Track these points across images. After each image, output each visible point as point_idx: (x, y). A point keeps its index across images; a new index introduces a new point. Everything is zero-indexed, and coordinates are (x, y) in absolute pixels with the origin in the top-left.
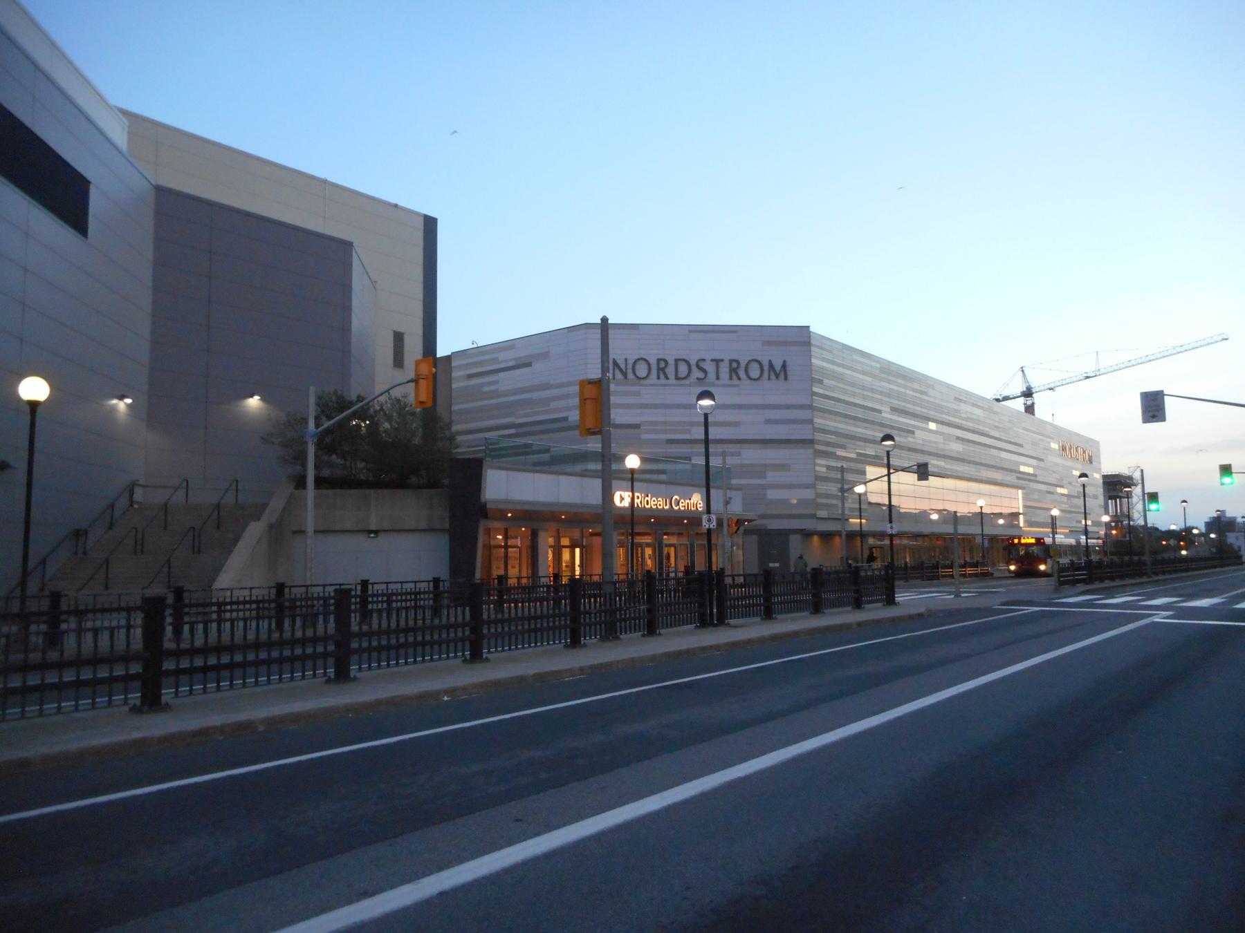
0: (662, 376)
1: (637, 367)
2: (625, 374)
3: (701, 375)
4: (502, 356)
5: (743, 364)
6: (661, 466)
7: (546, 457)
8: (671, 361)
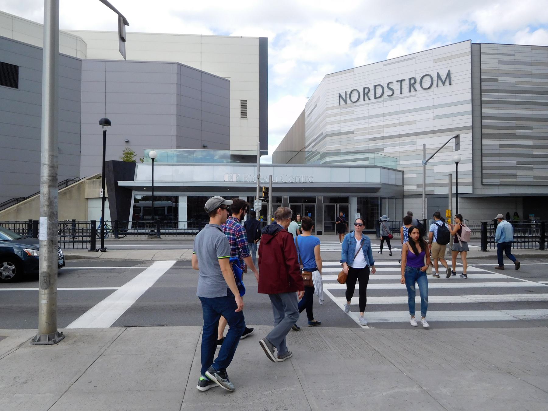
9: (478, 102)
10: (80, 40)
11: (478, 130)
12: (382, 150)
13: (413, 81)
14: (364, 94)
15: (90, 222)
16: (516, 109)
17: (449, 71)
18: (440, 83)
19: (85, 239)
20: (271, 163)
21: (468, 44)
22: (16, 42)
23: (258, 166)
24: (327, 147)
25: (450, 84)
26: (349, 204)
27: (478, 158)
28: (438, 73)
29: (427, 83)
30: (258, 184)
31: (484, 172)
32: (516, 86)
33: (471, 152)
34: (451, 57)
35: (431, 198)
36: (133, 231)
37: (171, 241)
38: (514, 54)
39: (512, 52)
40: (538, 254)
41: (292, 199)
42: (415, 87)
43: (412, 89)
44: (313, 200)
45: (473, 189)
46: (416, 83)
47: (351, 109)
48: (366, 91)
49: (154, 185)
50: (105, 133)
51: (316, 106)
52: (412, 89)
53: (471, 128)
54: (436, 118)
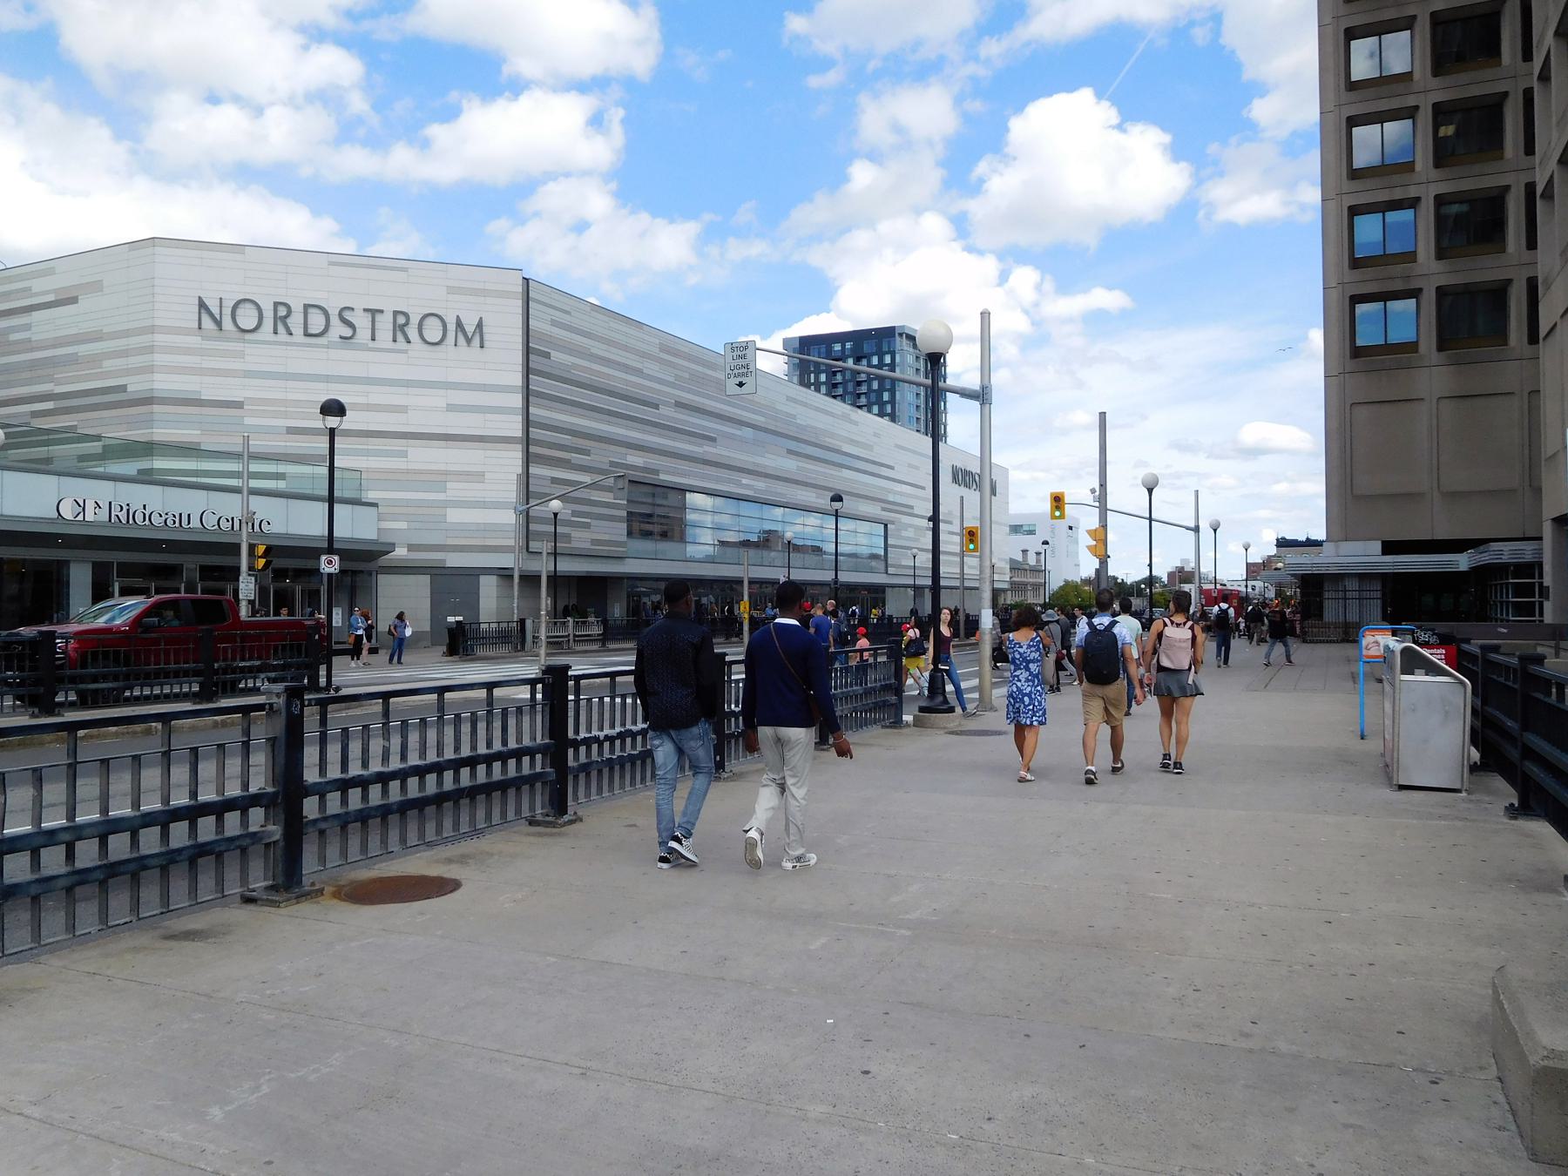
0: (281, 329)
1: (239, 312)
2: (219, 324)
3: (348, 332)
4: (37, 285)
5: (415, 320)
6: (282, 468)
7: (95, 447)
8: (297, 308)
43: (281, 329)
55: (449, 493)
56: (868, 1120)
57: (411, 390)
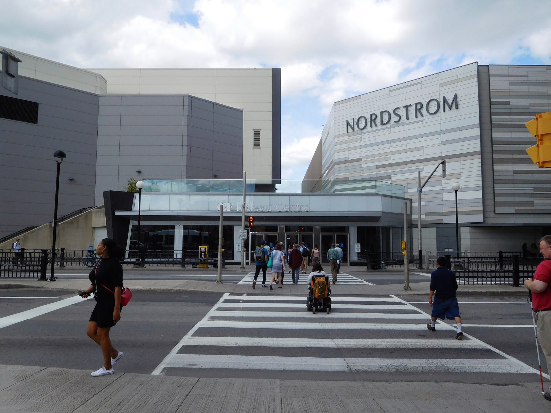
3: (397, 119)
9: (487, 126)
10: (100, 77)
11: (488, 155)
12: (389, 177)
13: (419, 107)
14: (371, 121)
15: (41, 251)
16: (511, 132)
17: (456, 95)
18: (447, 108)
19: (36, 268)
20: (300, 191)
21: (475, 67)
22: (39, 82)
23: (244, 195)
24: (335, 175)
25: (457, 108)
26: (348, 234)
27: (489, 184)
28: (444, 98)
29: (433, 109)
30: (243, 213)
31: (497, 199)
32: (530, 108)
33: (481, 178)
34: (457, 81)
35: (440, 227)
36: (129, 260)
37: (154, 270)
38: (527, 75)
39: (525, 73)
40: (506, 291)
41: (324, 229)
42: (422, 112)
43: (419, 115)
44: (310, 229)
45: (484, 217)
46: (423, 108)
47: (359, 136)
48: (374, 117)
49: (140, 215)
50: (59, 165)
51: (328, 133)
52: (419, 115)
53: (480, 153)
54: (443, 143)
55: (444, 186)
56: (115, 379)
57: (425, 139)
